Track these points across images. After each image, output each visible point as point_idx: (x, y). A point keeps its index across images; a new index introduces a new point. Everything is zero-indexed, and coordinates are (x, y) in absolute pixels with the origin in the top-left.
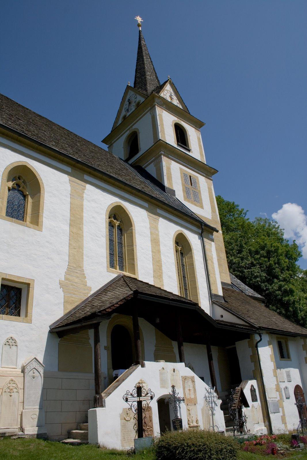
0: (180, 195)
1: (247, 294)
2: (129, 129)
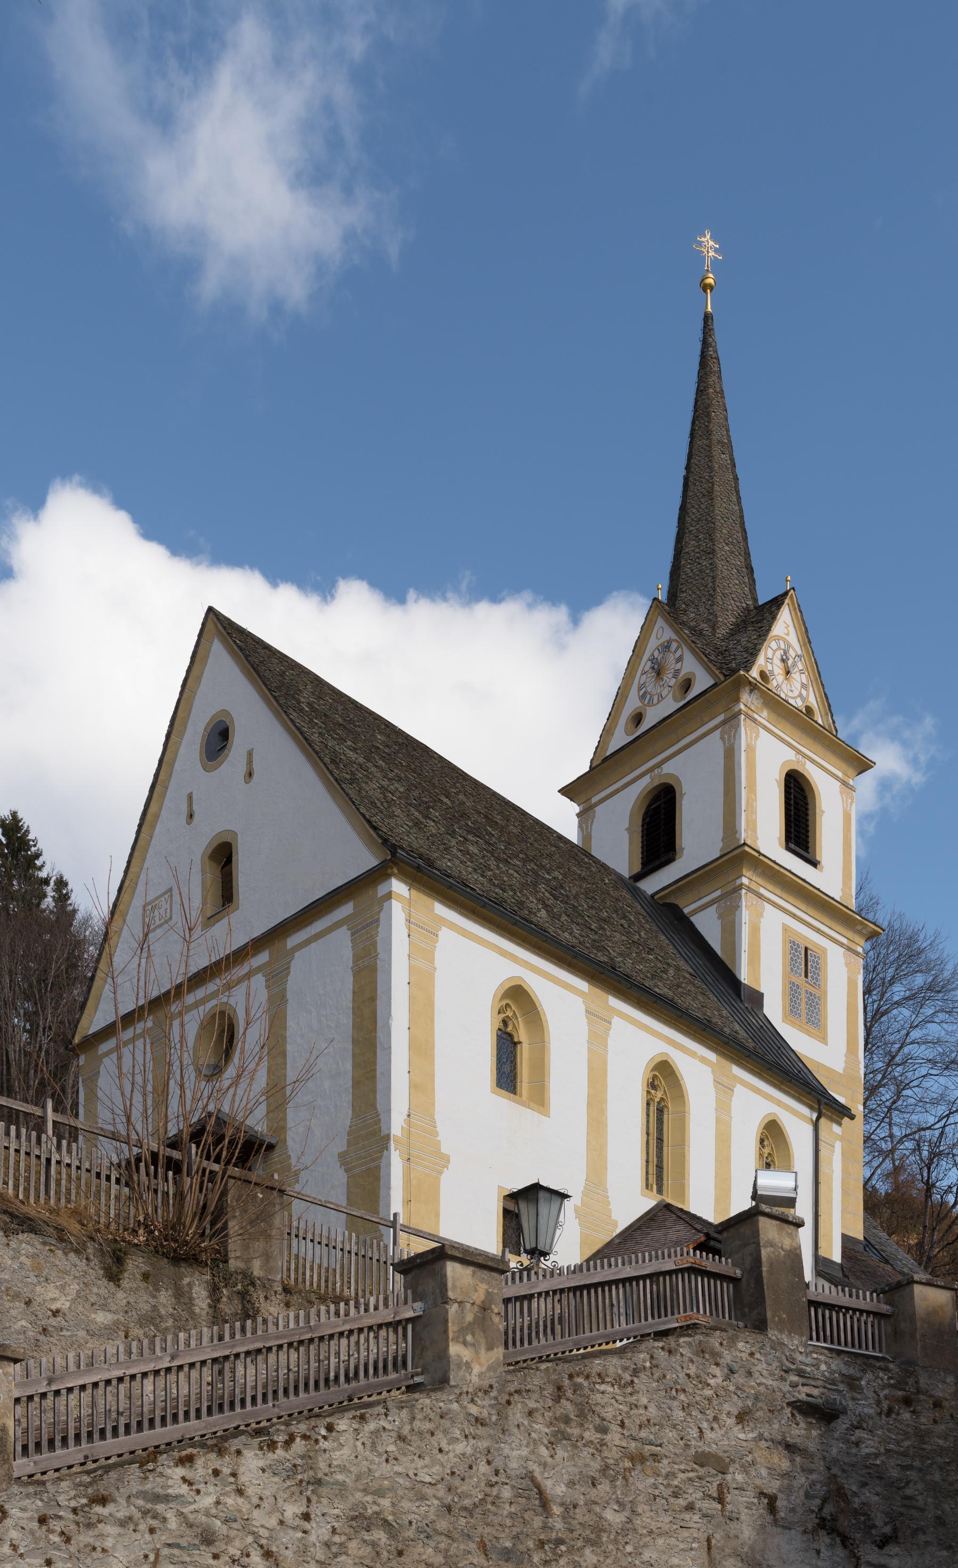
0: (774, 1009)
1: (898, 1269)
2: (651, 770)
